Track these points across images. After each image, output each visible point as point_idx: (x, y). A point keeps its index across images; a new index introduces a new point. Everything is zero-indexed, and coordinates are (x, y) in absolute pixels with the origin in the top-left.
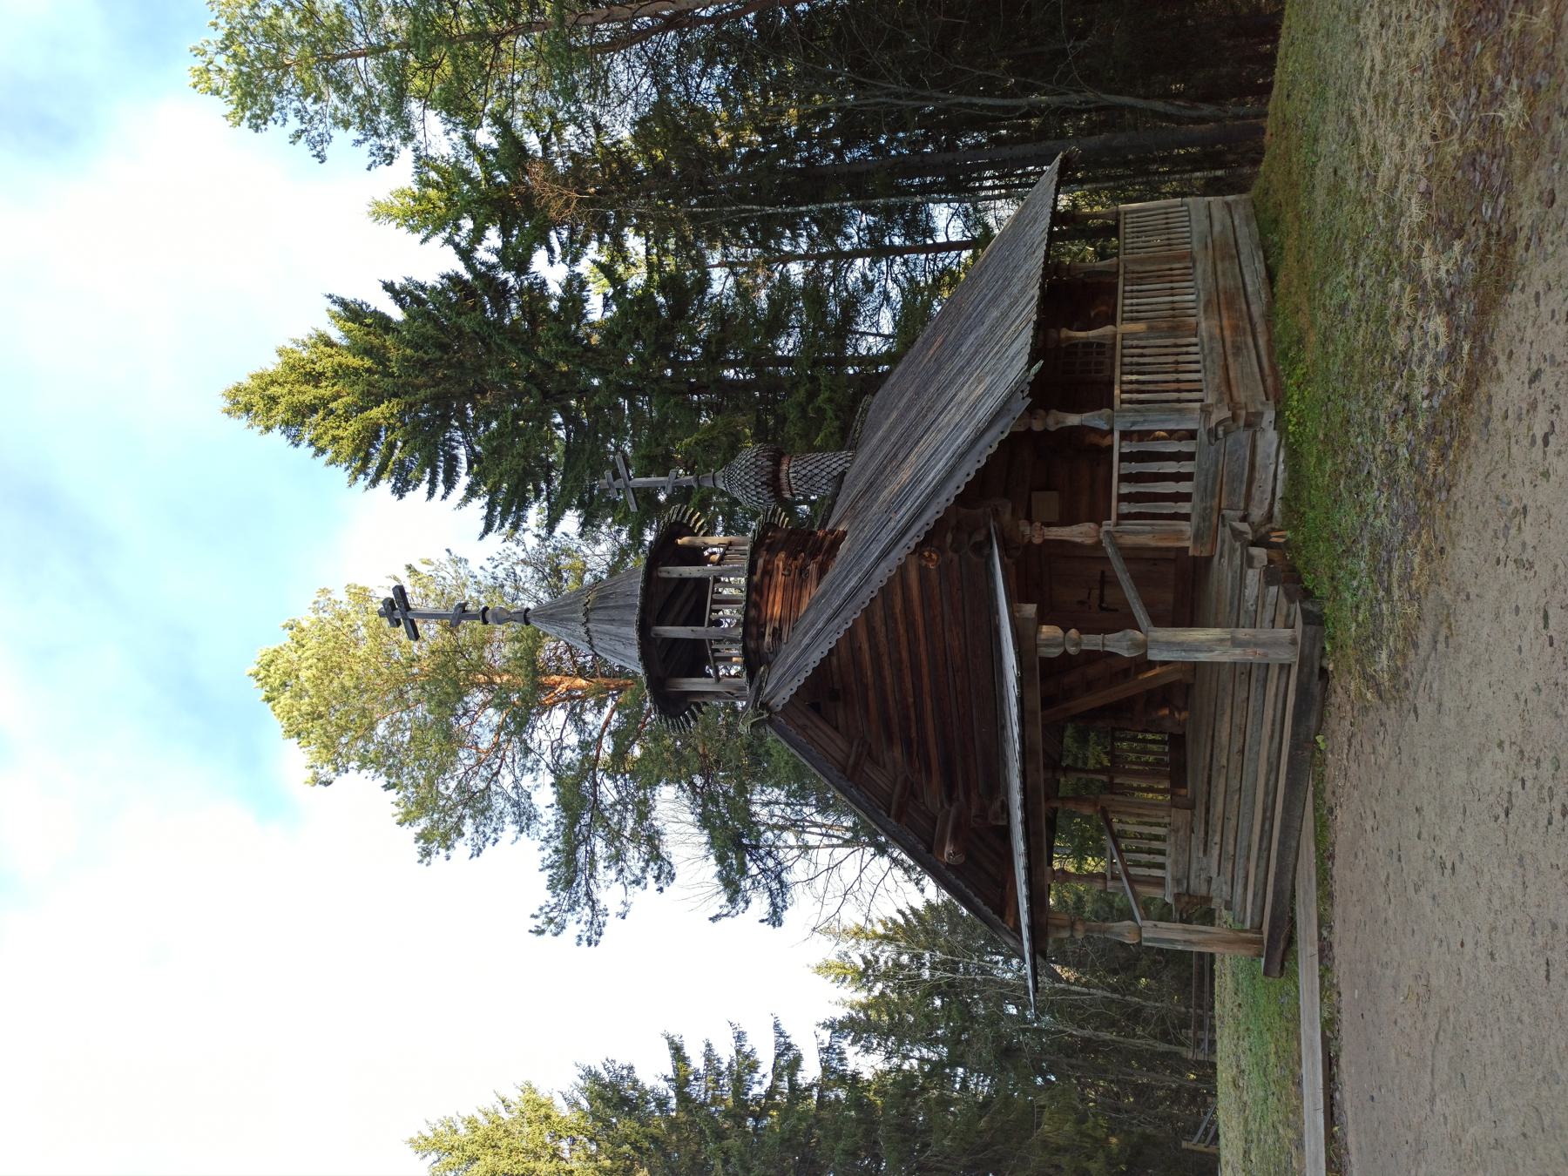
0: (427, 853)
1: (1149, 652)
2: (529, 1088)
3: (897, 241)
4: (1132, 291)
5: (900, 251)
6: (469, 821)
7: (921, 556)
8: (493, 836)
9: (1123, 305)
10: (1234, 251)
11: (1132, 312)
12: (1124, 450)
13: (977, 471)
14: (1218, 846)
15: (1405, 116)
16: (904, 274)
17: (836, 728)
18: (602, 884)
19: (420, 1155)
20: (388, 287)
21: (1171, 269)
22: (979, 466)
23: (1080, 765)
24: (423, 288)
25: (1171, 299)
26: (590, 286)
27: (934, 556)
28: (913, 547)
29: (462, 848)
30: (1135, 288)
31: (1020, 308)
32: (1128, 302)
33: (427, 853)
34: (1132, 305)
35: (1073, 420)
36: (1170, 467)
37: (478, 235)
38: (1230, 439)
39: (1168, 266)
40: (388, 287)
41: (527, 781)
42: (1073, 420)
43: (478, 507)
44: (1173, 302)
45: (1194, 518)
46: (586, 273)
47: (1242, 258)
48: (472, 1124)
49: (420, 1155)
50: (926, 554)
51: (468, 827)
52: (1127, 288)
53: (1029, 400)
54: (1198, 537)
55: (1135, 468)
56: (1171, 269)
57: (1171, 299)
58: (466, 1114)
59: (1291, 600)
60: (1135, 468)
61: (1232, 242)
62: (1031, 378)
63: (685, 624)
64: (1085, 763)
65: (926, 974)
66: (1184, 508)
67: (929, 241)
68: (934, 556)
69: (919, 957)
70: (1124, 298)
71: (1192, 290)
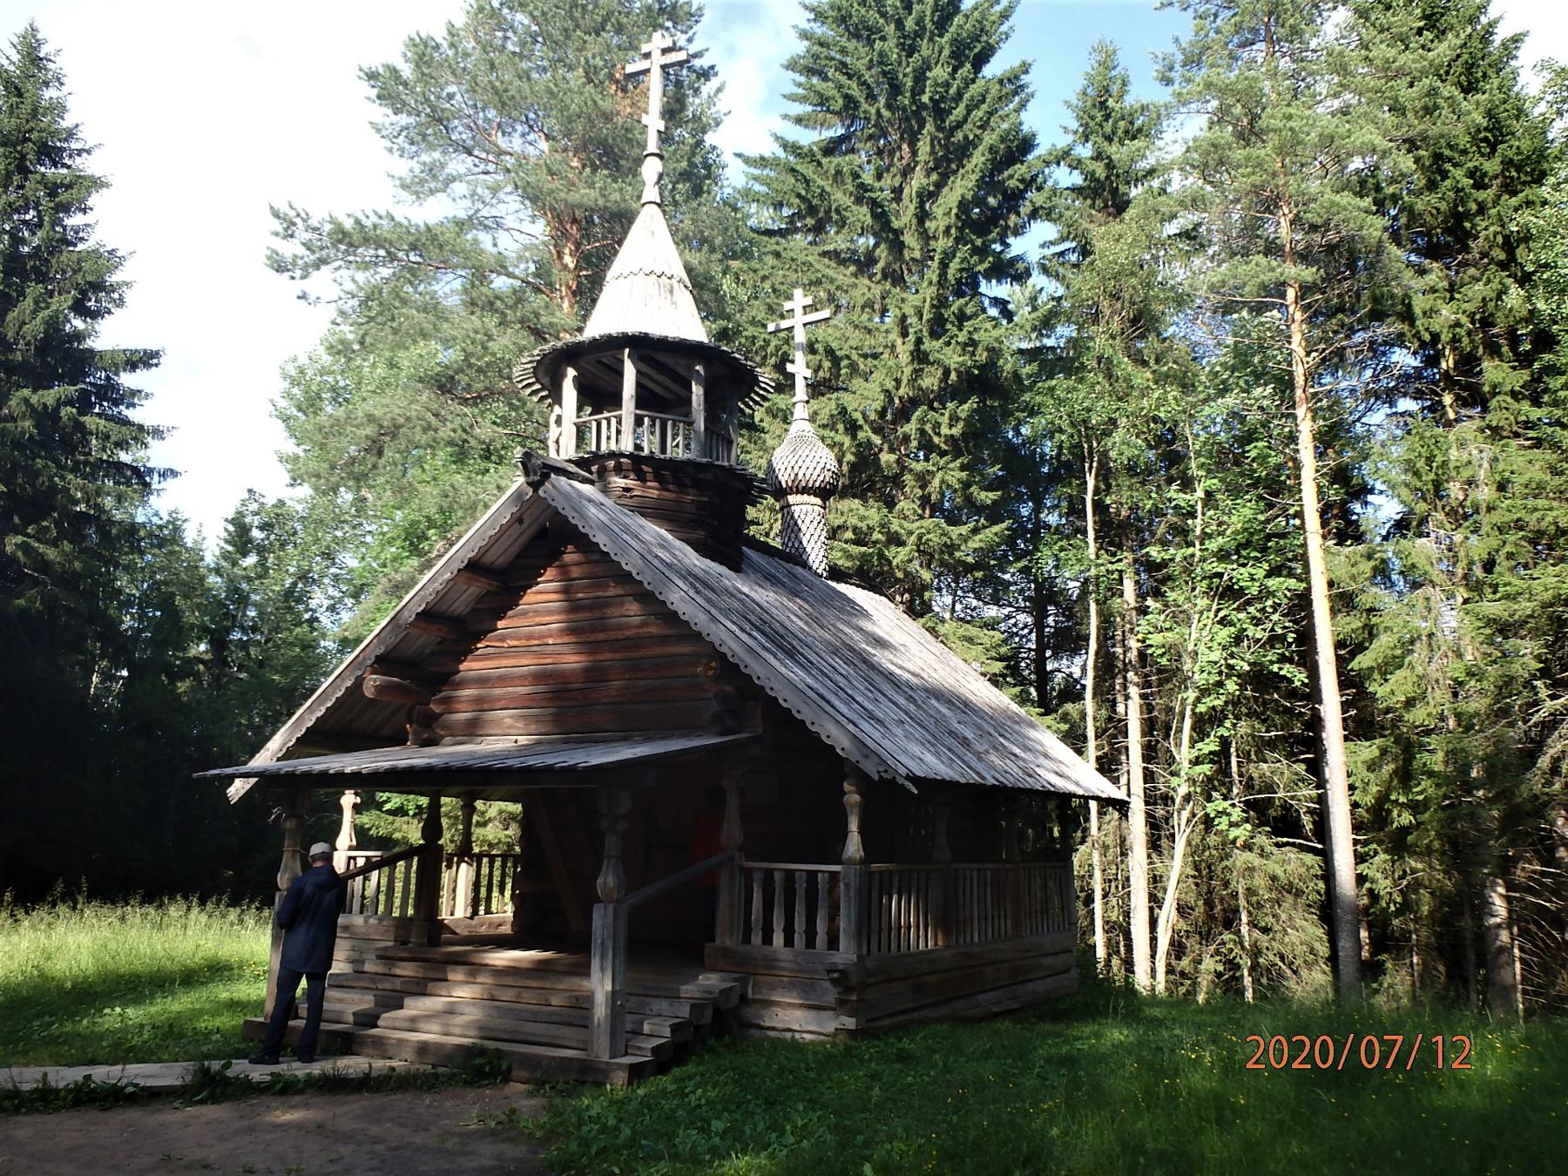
0: (372, 76)
1: (602, 905)
2: (97, 184)
3: (1050, 620)
4: (985, 878)
5: (1039, 624)
6: (412, 120)
7: (713, 659)
8: (395, 147)
9: (971, 870)
10: (1021, 979)
11: (965, 879)
12: (820, 875)
13: (803, 722)
14: (387, 971)
15: (859, 201)
16: (1015, 625)
17: (518, 557)
18: (338, 274)
19: (15, 41)
20: (1025, 68)
21: (1005, 916)
22: (808, 724)
23: (475, 818)
24: (1023, 106)
25: (976, 917)
26: (1017, 287)
27: (711, 673)
28: (722, 649)
29: (382, 114)
30: (989, 881)
31: (973, 764)
32: (975, 874)
33: (372, 76)
34: (971, 878)
35: (854, 826)
36: (799, 924)
37: (1076, 165)
38: (828, 985)
39: (1009, 913)
40: (1025, 68)
41: (459, 188)
42: (854, 826)
43: (772, 149)
44: (972, 919)
45: (743, 948)
46: (1031, 282)
47: (1014, 987)
48: (59, 108)
49: (15, 41)
50: (713, 664)
51: (404, 119)
52: (989, 873)
53: (876, 777)
54: (726, 952)
55: (801, 887)
56: (1005, 916)
57: (976, 917)
58: (70, 103)
59: (655, 1050)
60: (801, 887)
61: (1029, 977)
62: (900, 781)
63: (639, 385)
64: (479, 824)
65: (236, 635)
66: (757, 939)
67: (1049, 653)
68: (711, 673)
69: (254, 629)
70: (979, 870)
71: (983, 939)
